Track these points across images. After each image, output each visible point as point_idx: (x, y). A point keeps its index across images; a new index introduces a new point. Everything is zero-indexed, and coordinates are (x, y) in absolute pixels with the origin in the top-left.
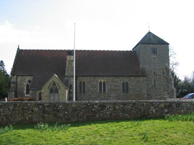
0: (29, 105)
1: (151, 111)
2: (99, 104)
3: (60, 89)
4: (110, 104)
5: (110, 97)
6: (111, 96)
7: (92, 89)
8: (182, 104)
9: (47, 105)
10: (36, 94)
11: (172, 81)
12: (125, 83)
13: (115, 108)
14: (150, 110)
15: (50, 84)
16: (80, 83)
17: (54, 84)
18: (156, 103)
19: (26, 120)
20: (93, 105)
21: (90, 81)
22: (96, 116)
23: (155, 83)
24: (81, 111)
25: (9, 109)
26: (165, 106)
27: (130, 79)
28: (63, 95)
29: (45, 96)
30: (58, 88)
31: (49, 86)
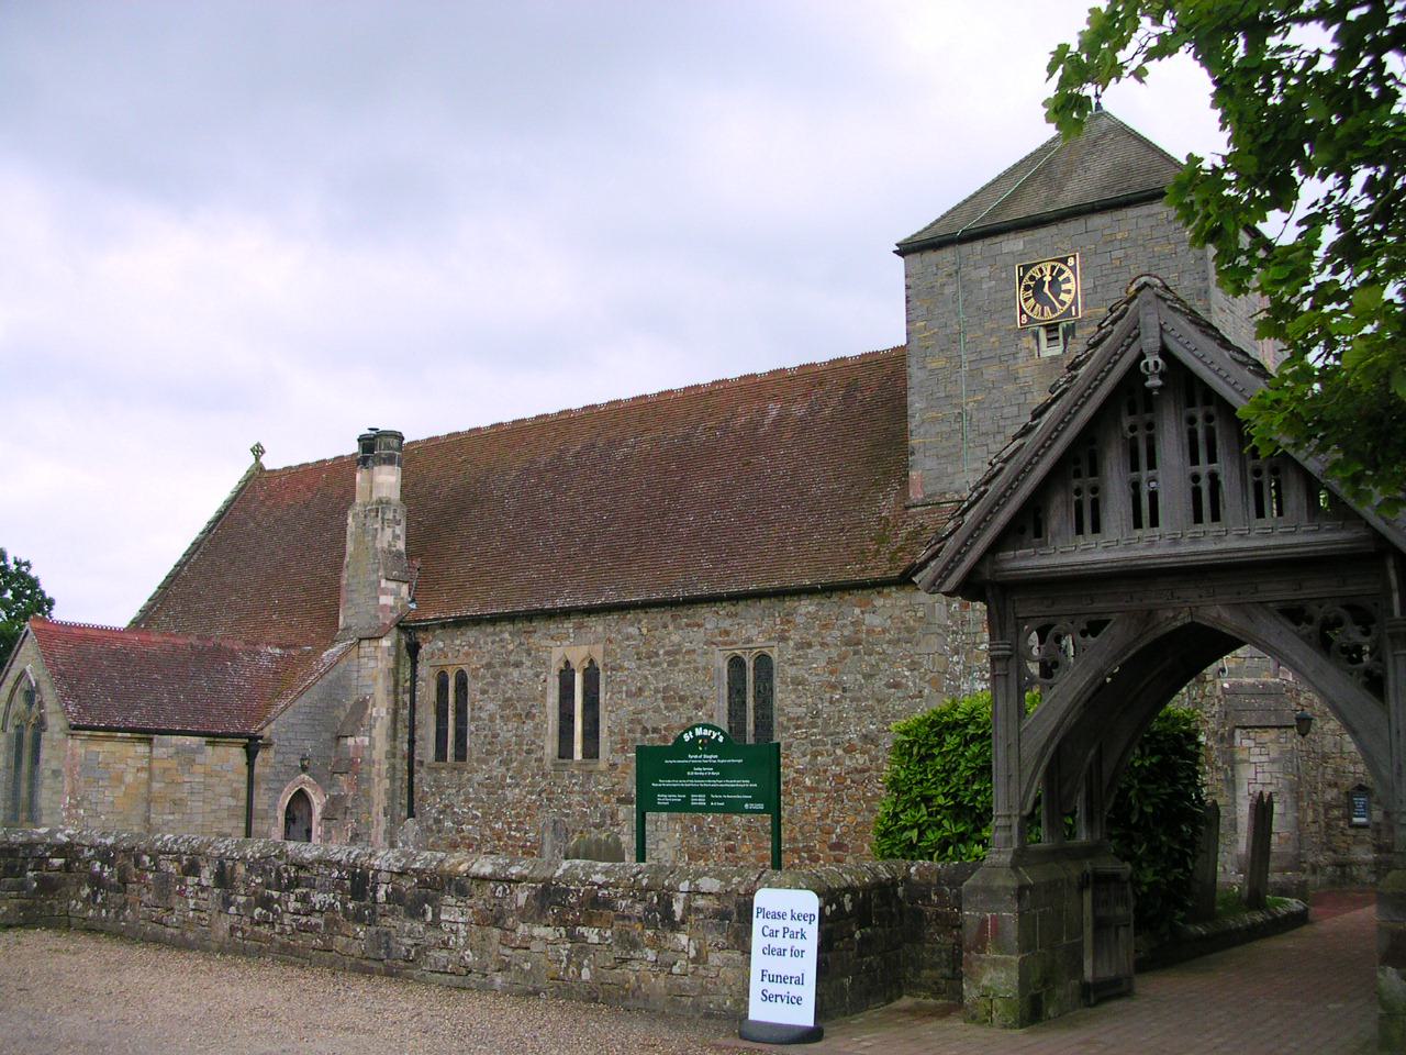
21: (496, 661)
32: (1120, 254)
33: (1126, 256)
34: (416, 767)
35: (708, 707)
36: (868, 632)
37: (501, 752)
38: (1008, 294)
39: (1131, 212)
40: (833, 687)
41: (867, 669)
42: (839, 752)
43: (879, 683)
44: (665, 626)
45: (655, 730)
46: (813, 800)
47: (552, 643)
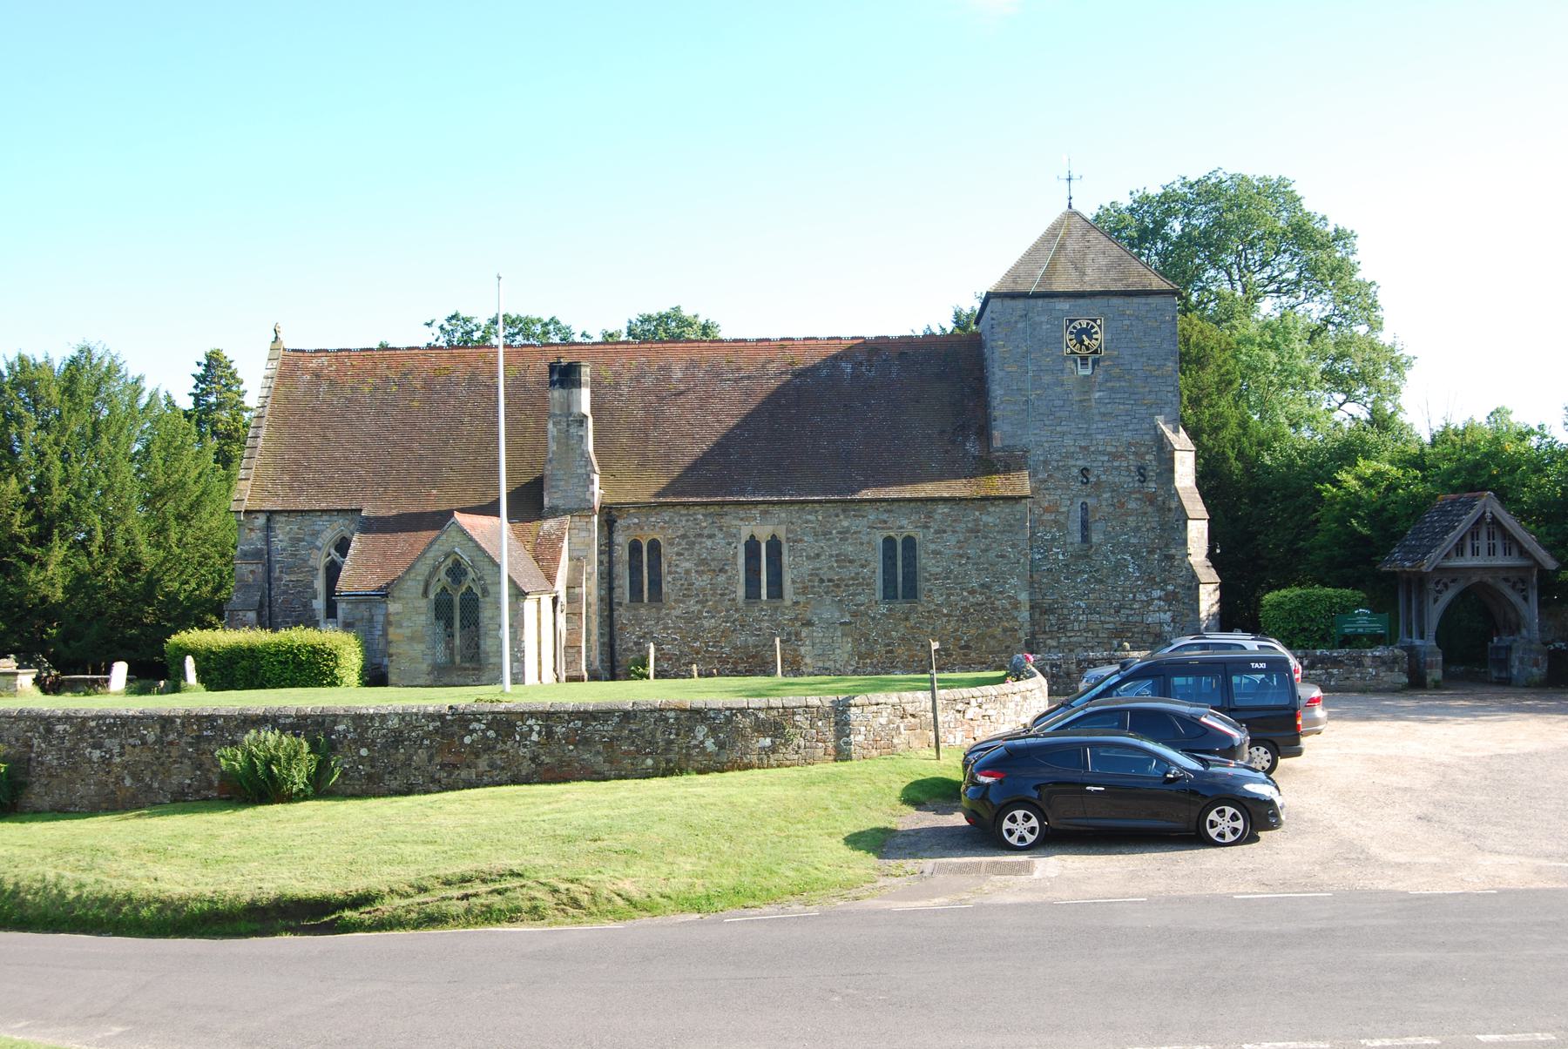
0: (220, 722)
1: (696, 746)
2: (490, 717)
5: (809, 623)
9: (288, 721)
10: (371, 620)
12: (899, 540)
14: (694, 742)
15: (436, 569)
16: (635, 548)
19: (210, 786)
20: (465, 721)
21: (691, 533)
24: (422, 744)
27: (929, 516)
29: (412, 639)
32: (1127, 322)
33: (1131, 325)
34: (615, 607)
35: (871, 566)
36: (984, 526)
37: (697, 595)
38: (1058, 335)
39: (1136, 300)
40: (961, 556)
41: (983, 547)
42: (965, 594)
43: (992, 554)
44: (837, 516)
45: (830, 580)
46: (948, 621)
47: (741, 523)
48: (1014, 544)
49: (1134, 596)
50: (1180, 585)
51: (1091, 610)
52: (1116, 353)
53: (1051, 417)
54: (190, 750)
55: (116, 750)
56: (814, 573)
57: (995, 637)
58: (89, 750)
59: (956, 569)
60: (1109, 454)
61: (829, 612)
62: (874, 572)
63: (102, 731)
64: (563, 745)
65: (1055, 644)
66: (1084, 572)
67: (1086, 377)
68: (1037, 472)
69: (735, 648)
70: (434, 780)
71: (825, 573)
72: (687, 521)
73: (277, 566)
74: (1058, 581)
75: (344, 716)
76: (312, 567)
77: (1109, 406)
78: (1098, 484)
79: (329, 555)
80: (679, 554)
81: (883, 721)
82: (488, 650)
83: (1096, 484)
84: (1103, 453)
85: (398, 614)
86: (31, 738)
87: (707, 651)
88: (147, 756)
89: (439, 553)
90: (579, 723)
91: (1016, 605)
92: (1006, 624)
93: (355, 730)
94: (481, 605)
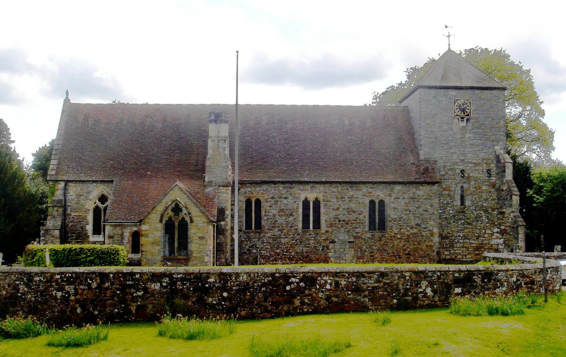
0: (138, 276)
1: (421, 292)
2: (301, 275)
3: (192, 221)
4: (327, 273)
5: (333, 242)
6: (336, 240)
7: (281, 220)
8: (497, 274)
9: (179, 276)
10: (122, 235)
11: (514, 197)
13: (337, 284)
14: (420, 290)
15: (167, 208)
17: (177, 209)
18: (434, 272)
22: (293, 303)
23: (462, 203)
25: (89, 285)
26: (454, 280)
27: (392, 190)
28: (201, 238)
29: (153, 243)
30: (188, 219)
31: (162, 216)
37: (279, 227)
40: (406, 210)
42: (408, 228)
43: (421, 210)
44: (347, 189)
45: (343, 221)
46: (400, 242)
47: (301, 192)
48: (432, 205)
49: (485, 231)
50: (508, 226)
51: (465, 237)
52: (477, 116)
53: (447, 145)
54: (118, 292)
55: (72, 291)
56: (336, 218)
57: (422, 250)
58: (55, 292)
59: (404, 217)
60: (474, 163)
61: (342, 236)
62: (365, 217)
63: (63, 281)
64: (345, 291)
65: (448, 254)
66: (462, 219)
67: (464, 127)
68: (440, 171)
69: (297, 253)
70: (267, 311)
71: (342, 217)
72: (275, 190)
73: (69, 208)
74: (450, 224)
75: (213, 274)
76: (87, 209)
77: (474, 141)
78: (469, 177)
79: (95, 203)
80: (270, 207)
81: (514, 279)
82: (192, 250)
83: (467, 177)
84: (471, 163)
85: (146, 230)
86: (18, 285)
87: (283, 255)
88: (90, 296)
89: (168, 200)
90: (354, 279)
91: (432, 234)
92: (428, 243)
93: (220, 282)
94: (189, 227)
